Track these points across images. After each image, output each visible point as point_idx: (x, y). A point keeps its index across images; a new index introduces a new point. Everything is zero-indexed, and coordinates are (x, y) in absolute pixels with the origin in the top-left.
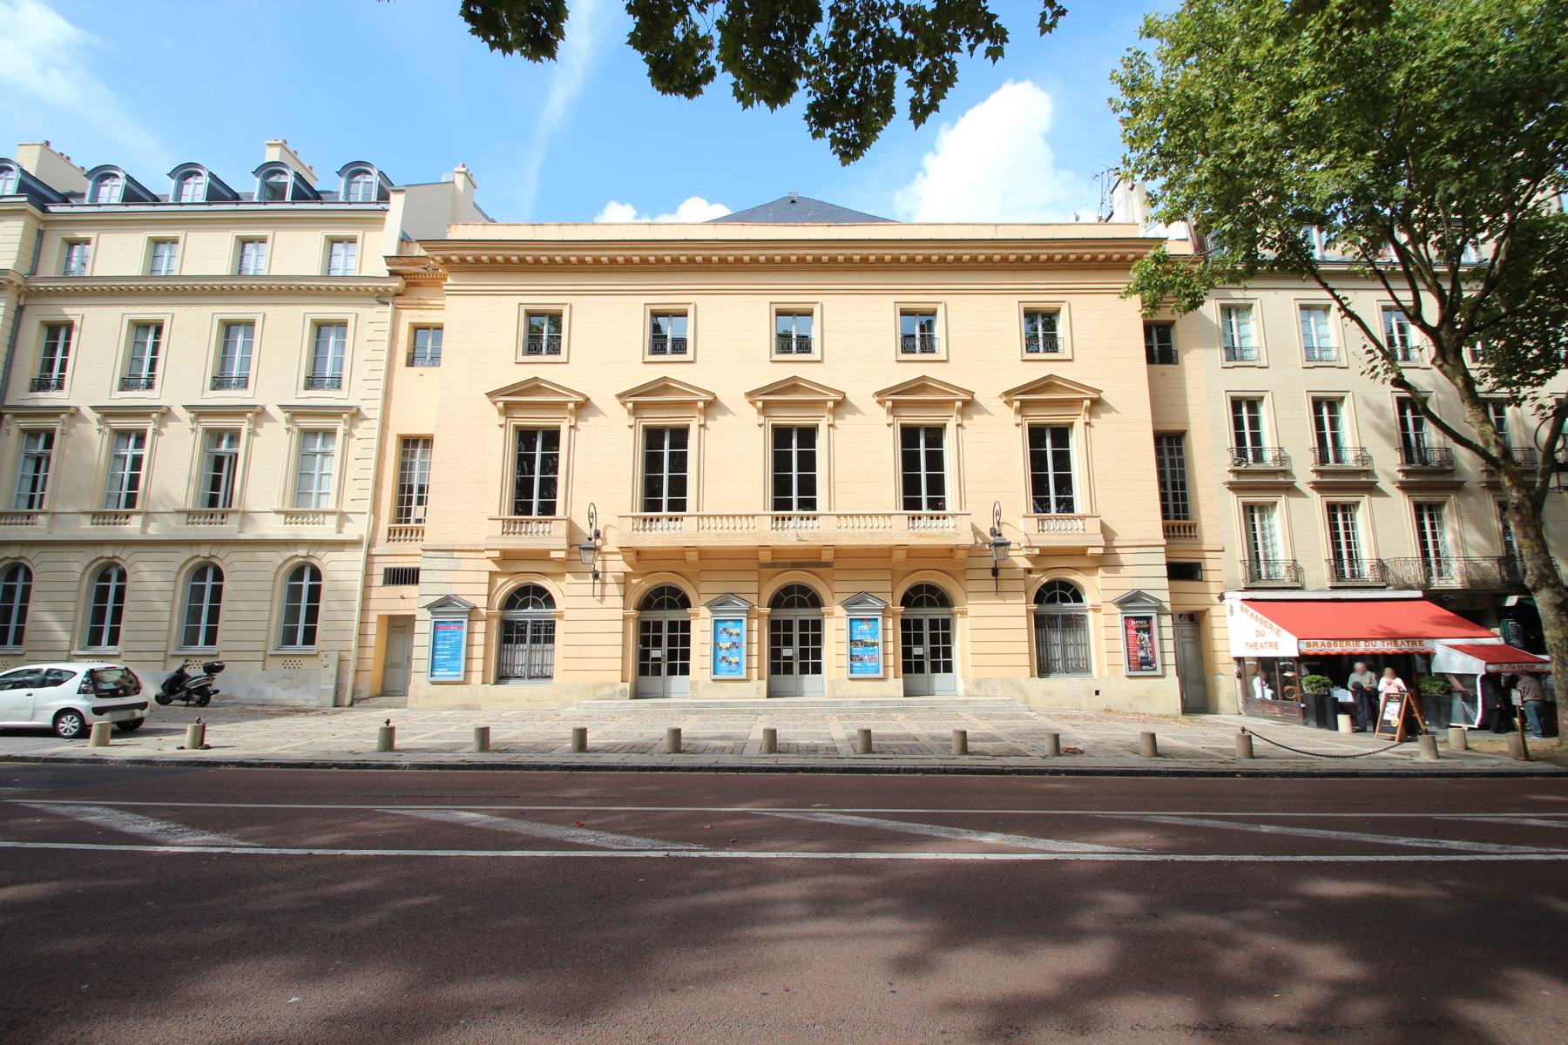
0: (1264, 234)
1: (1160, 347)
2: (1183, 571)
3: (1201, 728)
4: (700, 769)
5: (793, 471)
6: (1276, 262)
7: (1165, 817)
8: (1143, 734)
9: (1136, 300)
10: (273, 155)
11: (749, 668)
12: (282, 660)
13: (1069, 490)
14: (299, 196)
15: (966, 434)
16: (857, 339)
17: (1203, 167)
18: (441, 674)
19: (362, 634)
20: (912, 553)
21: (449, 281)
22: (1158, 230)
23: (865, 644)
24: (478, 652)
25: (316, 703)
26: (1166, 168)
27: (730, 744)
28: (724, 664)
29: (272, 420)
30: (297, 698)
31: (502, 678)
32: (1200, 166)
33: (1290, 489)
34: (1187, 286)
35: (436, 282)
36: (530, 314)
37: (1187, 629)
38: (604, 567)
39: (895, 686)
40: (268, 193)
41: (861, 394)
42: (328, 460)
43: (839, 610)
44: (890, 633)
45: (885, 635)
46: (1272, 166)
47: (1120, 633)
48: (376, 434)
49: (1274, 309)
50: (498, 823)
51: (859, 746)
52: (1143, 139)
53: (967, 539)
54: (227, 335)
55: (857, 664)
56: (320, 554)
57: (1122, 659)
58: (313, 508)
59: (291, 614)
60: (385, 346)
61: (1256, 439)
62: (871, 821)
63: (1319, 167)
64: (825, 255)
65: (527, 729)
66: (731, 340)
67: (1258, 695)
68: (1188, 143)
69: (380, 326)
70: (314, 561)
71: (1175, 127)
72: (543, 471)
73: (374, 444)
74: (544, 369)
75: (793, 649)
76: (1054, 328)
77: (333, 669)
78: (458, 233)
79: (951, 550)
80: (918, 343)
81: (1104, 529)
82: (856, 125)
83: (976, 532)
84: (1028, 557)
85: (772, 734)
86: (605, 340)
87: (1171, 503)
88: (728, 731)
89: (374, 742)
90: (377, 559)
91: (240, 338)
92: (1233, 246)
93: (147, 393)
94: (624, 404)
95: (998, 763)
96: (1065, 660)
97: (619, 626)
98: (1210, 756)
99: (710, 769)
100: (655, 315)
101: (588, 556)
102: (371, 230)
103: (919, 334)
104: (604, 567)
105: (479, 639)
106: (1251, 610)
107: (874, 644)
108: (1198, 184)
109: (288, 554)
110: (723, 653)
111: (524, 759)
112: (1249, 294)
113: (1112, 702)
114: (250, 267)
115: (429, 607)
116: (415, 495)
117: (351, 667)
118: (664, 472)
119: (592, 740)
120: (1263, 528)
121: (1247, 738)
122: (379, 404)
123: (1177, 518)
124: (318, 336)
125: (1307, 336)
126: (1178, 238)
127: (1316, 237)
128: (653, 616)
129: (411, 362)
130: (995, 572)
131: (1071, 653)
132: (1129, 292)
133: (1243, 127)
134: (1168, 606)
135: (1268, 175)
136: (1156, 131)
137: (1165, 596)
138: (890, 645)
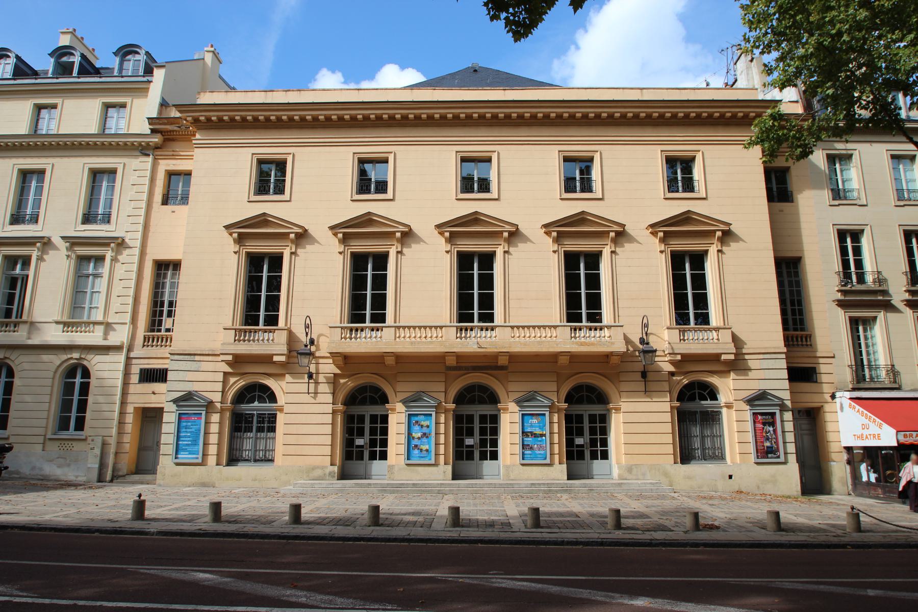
0: (860, 98)
1: (779, 189)
2: (802, 374)
3: (818, 507)
4: (395, 540)
6: (870, 120)
7: (788, 583)
8: (769, 512)
9: (757, 150)
10: (65, 40)
11: (437, 455)
12: (58, 443)
13: (706, 306)
14: (83, 71)
16: (527, 181)
17: (808, 45)
18: (184, 456)
19: (121, 423)
20: (574, 358)
21: (198, 136)
22: (774, 94)
23: (534, 435)
24: (213, 439)
25: (84, 479)
26: (779, 45)
27: (421, 519)
28: (416, 451)
29: (56, 248)
30: (70, 475)
31: (233, 460)
32: (806, 43)
33: (888, 306)
35: (187, 138)
36: (261, 162)
37: (805, 423)
38: (317, 369)
39: (559, 471)
40: (60, 71)
42: (98, 280)
44: (556, 426)
45: (551, 428)
46: (865, 43)
47: (749, 426)
48: (136, 259)
49: (869, 160)
50: (226, 583)
52: (759, 22)
54: (24, 182)
55: (527, 452)
56: (89, 357)
57: (751, 448)
58: (85, 319)
59: (66, 406)
61: (859, 264)
62: (540, 586)
63: (902, 45)
64: (501, 113)
65: (254, 504)
66: (424, 183)
67: (865, 479)
68: (796, 25)
70: (85, 363)
71: (786, 12)
72: (269, 289)
73: (135, 267)
74: (272, 207)
75: (473, 442)
76: (691, 172)
77: (97, 451)
78: (206, 98)
79: (607, 356)
80: (578, 184)
81: (735, 338)
82: (526, 10)
83: (627, 341)
84: (672, 363)
85: (455, 511)
87: (790, 317)
88: (419, 508)
89: (128, 513)
90: (134, 361)
91: (34, 184)
92: (835, 108)
93: (31, 227)
95: (647, 536)
97: (329, 419)
98: (825, 531)
99: (403, 540)
100: (362, 161)
101: (305, 360)
102: (139, 97)
103: (578, 176)
104: (317, 369)
105: (214, 428)
106: (858, 407)
107: (542, 435)
109: (65, 357)
110: (414, 442)
111: (250, 528)
112: (850, 146)
113: (745, 483)
114: (43, 129)
115: (175, 401)
116: (166, 309)
117: (112, 450)
118: (367, 289)
119: (305, 514)
120: (866, 338)
121: (855, 515)
122: (139, 235)
123: (796, 330)
124: (94, 182)
125: (897, 180)
126: (790, 100)
127: (902, 100)
128: (357, 410)
129: (165, 201)
130: (644, 374)
131: (708, 443)
132: (751, 144)
133: (840, 13)
134: (789, 403)
135: (861, 51)
136: (769, 15)
137: (786, 396)
138: (556, 437)
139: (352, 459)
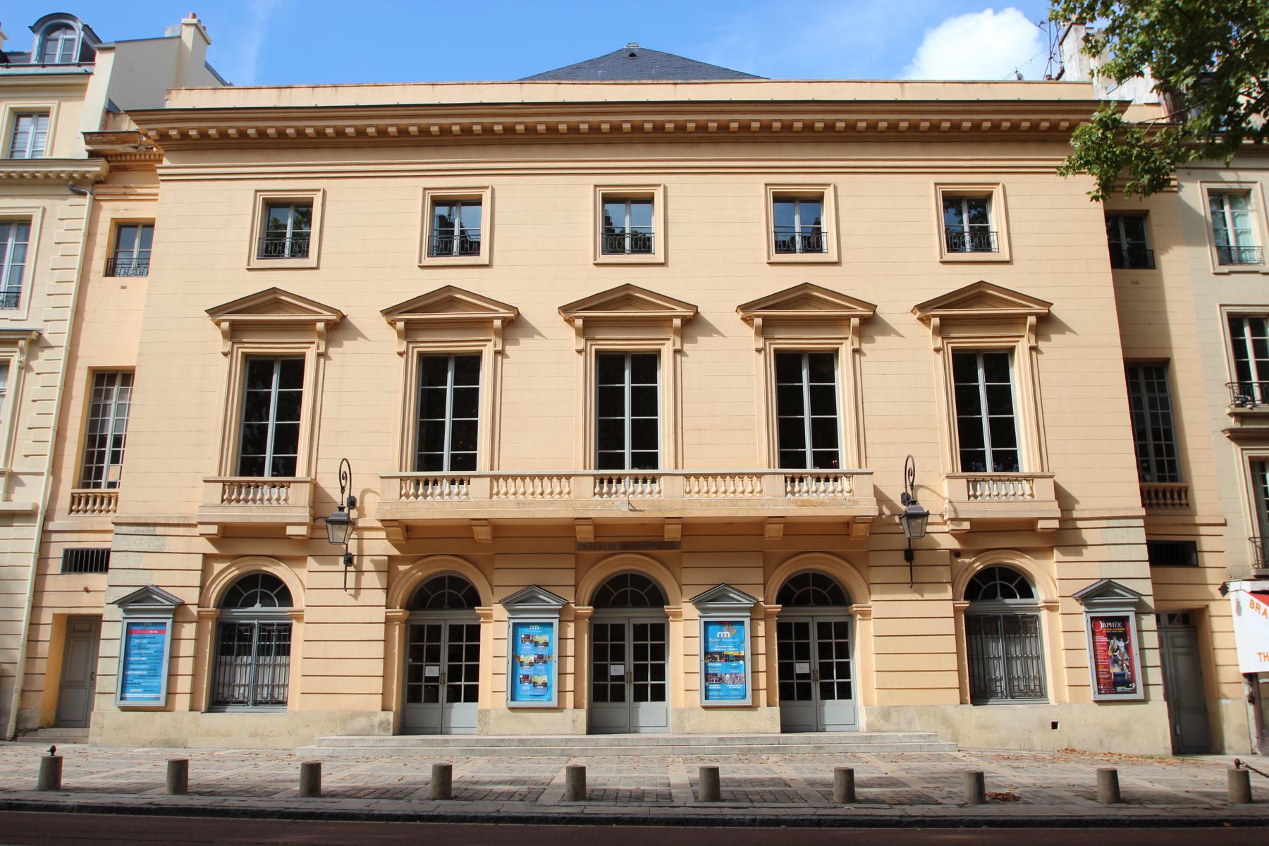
1: (1131, 247)
2: (1173, 553)
4: (474, 819)
5: (625, 415)
11: (561, 691)
15: (866, 363)
16: (714, 236)
18: (135, 696)
20: (793, 528)
21: (166, 162)
23: (725, 658)
24: (185, 666)
27: (524, 788)
28: (526, 686)
31: (218, 702)
34: (1147, 159)
36: (270, 205)
37: (1179, 635)
38: (360, 548)
39: (768, 718)
41: (720, 309)
43: (689, 610)
47: (1085, 640)
48: (60, 366)
51: (701, 790)
53: (868, 508)
55: (714, 686)
57: (1089, 677)
60: (79, 250)
66: (540, 237)
69: (73, 225)
73: (58, 380)
74: (287, 278)
75: (623, 670)
78: (181, 100)
79: (847, 525)
83: (880, 498)
84: (956, 535)
86: (370, 236)
90: (54, 537)
94: (392, 323)
96: (1010, 679)
101: (338, 534)
102: (70, 99)
104: (360, 548)
105: (187, 648)
107: (738, 658)
108: (1149, 29)
110: (522, 671)
111: (233, 802)
112: (1245, 176)
116: (109, 449)
118: (445, 417)
119: (327, 782)
122: (66, 327)
123: (1162, 479)
126: (1142, 98)
128: (429, 618)
129: (111, 271)
130: (909, 555)
131: (1018, 669)
134: (1150, 601)
137: (1145, 588)
138: (762, 661)
139: (419, 701)
